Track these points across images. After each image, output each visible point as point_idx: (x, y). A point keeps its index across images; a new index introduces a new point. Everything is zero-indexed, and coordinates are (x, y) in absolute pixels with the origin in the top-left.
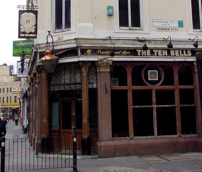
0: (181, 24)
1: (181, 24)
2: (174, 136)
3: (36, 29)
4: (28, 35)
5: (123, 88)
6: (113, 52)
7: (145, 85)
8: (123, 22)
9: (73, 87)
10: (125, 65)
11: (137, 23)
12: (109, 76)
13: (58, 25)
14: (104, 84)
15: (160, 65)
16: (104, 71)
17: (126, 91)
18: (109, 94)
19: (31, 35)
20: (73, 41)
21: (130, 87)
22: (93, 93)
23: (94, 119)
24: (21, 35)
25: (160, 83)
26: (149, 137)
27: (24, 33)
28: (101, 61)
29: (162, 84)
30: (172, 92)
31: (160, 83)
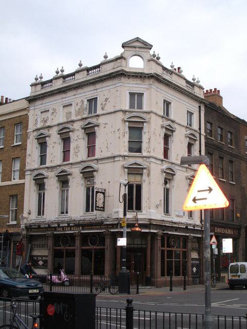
3: (104, 205)
9: (136, 246)
20: (147, 220)
27: (98, 207)
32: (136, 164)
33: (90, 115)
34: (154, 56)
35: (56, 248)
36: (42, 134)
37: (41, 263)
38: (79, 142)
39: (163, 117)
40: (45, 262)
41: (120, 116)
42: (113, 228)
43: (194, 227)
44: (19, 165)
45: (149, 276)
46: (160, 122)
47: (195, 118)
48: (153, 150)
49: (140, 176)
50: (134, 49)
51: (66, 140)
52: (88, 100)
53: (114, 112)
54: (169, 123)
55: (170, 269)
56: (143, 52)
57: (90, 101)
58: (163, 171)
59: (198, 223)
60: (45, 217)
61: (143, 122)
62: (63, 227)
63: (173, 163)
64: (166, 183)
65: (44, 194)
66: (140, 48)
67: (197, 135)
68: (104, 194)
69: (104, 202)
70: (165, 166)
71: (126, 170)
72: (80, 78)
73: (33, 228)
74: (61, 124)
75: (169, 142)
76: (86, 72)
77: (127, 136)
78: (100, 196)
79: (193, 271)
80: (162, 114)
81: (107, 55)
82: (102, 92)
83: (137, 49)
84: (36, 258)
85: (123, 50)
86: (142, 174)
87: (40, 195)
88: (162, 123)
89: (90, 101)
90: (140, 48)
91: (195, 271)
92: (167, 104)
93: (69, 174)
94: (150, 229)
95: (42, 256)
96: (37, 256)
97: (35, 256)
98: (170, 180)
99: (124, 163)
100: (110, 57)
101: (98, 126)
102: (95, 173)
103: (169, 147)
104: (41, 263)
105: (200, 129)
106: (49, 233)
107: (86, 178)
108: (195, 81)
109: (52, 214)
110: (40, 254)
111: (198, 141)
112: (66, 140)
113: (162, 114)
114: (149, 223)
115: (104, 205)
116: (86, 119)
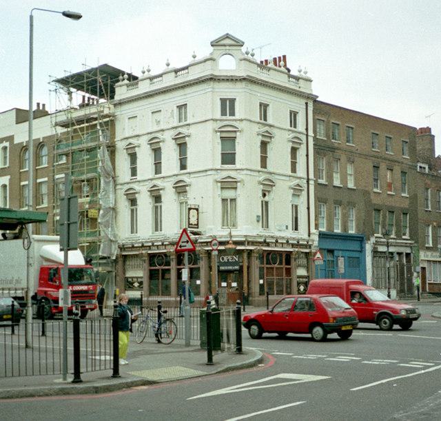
3: (198, 222)
32: (229, 177)
33: (181, 124)
34: (247, 53)
35: (152, 268)
36: (130, 144)
37: (136, 285)
38: (170, 155)
39: (259, 123)
40: (141, 283)
41: (211, 126)
42: (207, 246)
44: (47, 150)
45: (246, 295)
46: (256, 128)
47: (301, 119)
50: (223, 48)
51: (157, 152)
52: (178, 107)
53: (206, 121)
54: (267, 128)
56: (234, 50)
57: (179, 107)
58: (260, 183)
59: (305, 236)
60: (138, 235)
61: (235, 131)
62: (157, 246)
64: (264, 195)
65: (136, 209)
66: (230, 45)
67: (304, 138)
68: (197, 210)
70: (262, 177)
71: (219, 184)
72: (169, 81)
73: (127, 248)
74: (151, 133)
75: (268, 149)
76: (173, 73)
77: (219, 147)
78: (193, 212)
79: (299, 290)
80: (258, 120)
81: (196, 54)
82: (192, 97)
83: (228, 48)
84: (130, 280)
85: (212, 48)
87: (132, 211)
88: (258, 130)
89: (179, 107)
90: (230, 45)
91: (302, 290)
92: (264, 107)
93: (161, 189)
95: (137, 278)
96: (132, 278)
97: (130, 278)
98: (269, 192)
99: (216, 177)
100: (200, 58)
101: (189, 136)
102: (187, 188)
104: (136, 285)
105: (307, 129)
106: (144, 252)
107: (179, 193)
108: (302, 73)
109: (145, 232)
110: (134, 275)
111: (305, 144)
112: (157, 152)
113: (258, 120)
115: (198, 222)
116: (176, 128)
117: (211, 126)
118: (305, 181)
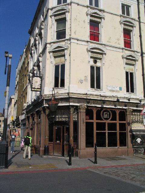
0: (121, 89)
1: (121, 89)
2: (116, 147)
3: (41, 87)
4: (36, 90)
5: (91, 121)
6: (104, 102)
7: (103, 120)
8: (92, 86)
10: (93, 109)
11: (99, 87)
12: (85, 114)
13: (56, 85)
14: (82, 119)
15: (111, 110)
16: (82, 111)
17: (93, 123)
18: (85, 124)
19: (38, 90)
21: (95, 121)
22: (76, 124)
23: (76, 138)
24: (33, 89)
25: (110, 119)
26: (104, 148)
27: (34, 88)
28: (81, 105)
29: (111, 120)
30: (115, 124)
31: (110, 119)
32: (59, 47)
43: (129, 100)
48: (75, 32)
49: (63, 58)
55: (101, 136)
63: (134, 51)
68: (41, 77)
69: (41, 85)
86: (64, 56)
94: (69, 102)
103: (100, 32)
114: (68, 96)
115: (41, 87)
117: (118, 19)
118: (140, 54)
